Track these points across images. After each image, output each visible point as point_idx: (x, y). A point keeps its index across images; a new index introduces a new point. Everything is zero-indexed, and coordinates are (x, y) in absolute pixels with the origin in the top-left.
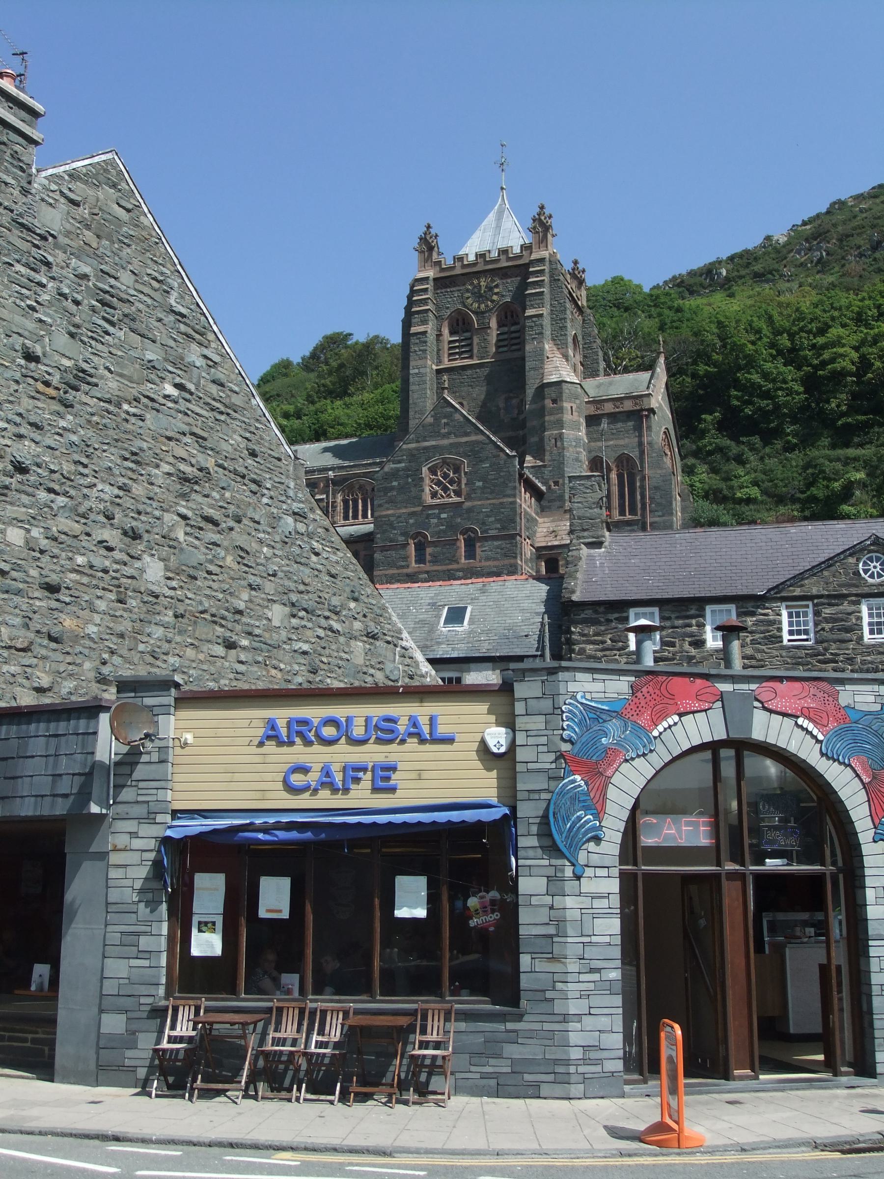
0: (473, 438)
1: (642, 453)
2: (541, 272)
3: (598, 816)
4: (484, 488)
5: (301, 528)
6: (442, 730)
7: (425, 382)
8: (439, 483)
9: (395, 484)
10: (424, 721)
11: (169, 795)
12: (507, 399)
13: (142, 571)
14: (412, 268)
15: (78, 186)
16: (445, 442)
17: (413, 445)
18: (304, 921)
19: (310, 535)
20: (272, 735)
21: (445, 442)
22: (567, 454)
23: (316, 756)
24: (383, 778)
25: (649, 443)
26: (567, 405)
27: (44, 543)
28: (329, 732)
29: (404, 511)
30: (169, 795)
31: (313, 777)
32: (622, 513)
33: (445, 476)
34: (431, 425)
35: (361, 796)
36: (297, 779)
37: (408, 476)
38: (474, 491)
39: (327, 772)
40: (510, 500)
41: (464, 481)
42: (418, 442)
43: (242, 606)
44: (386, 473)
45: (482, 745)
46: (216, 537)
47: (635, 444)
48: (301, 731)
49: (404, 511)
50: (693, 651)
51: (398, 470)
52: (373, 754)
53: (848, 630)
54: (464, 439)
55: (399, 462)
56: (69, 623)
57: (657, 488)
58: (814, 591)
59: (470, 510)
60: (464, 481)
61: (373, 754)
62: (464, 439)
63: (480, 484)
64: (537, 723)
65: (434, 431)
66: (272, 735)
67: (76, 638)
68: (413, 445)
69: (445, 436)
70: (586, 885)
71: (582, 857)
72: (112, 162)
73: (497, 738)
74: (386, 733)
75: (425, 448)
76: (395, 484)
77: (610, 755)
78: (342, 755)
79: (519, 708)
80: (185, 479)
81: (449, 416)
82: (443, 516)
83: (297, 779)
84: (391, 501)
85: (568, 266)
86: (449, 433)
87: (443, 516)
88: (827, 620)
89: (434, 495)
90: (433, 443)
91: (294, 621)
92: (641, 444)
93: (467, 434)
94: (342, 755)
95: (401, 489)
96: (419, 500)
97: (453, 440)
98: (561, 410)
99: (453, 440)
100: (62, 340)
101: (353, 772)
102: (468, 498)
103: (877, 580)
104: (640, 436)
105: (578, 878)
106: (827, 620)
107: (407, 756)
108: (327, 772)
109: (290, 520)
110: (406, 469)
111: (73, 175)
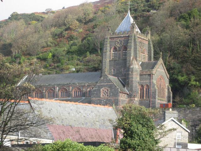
0: (111, 84)
1: (150, 85)
2: (113, 57)
4: (113, 95)
7: (106, 65)
8: (104, 93)
9: (95, 93)
12: (124, 69)
16: (105, 84)
17: (99, 84)
21: (105, 84)
22: (134, 85)
25: (152, 82)
26: (134, 73)
29: (97, 99)
32: (146, 98)
33: (105, 91)
34: (103, 80)
37: (98, 91)
38: (110, 95)
40: (117, 98)
41: (109, 93)
42: (100, 83)
44: (94, 90)
45: (175, 96)
47: (149, 82)
49: (97, 99)
51: (96, 89)
54: (109, 84)
55: (96, 88)
57: (153, 93)
60: (109, 93)
62: (109, 84)
63: (112, 94)
68: (99, 84)
69: (105, 83)
75: (101, 85)
76: (95, 93)
81: (106, 78)
82: (105, 101)
86: (106, 82)
87: (105, 101)
89: (103, 96)
90: (103, 84)
92: (150, 82)
93: (109, 83)
95: (97, 94)
96: (100, 97)
97: (107, 84)
98: (133, 74)
104: (150, 80)
110: (97, 90)
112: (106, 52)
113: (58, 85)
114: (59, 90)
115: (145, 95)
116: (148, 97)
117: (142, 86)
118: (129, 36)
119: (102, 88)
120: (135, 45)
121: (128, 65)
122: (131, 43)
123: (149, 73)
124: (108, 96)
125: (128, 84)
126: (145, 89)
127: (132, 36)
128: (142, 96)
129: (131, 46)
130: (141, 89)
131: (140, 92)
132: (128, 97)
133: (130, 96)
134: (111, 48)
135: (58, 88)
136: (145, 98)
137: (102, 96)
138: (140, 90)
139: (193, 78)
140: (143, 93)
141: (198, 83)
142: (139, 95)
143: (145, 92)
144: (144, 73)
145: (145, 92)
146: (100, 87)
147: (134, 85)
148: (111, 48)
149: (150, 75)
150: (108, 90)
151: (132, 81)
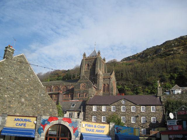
3: (43, 131)
5: (44, 95)
6: (31, 121)
10: (29, 120)
11: (5, 125)
13: (22, 100)
14: (82, 58)
15: (18, 58)
18: (22, 137)
19: (45, 96)
20: (15, 120)
23: (19, 122)
24: (25, 125)
27: (9, 97)
28: (21, 120)
30: (5, 125)
31: (18, 124)
32: (107, 91)
35: (23, 127)
36: (17, 124)
39: (20, 124)
43: (35, 104)
46: (32, 96)
48: (18, 120)
50: (100, 111)
52: (24, 122)
53: (120, 110)
56: (11, 106)
58: (116, 104)
59: (86, 90)
61: (24, 122)
64: (39, 121)
65: (82, 79)
66: (15, 120)
67: (12, 107)
69: (84, 80)
70: (41, 137)
71: (41, 135)
72: (23, 55)
73: (35, 122)
74: (25, 120)
77: (46, 125)
78: (22, 122)
79: (37, 119)
80: (28, 90)
83: (17, 124)
84: (76, 88)
85: (103, 58)
88: (117, 108)
91: (42, 106)
92: (110, 83)
94: (22, 122)
95: (78, 87)
97: (85, 81)
99: (85, 81)
100: (14, 75)
101: (22, 124)
102: (86, 89)
103: (124, 104)
105: (40, 136)
106: (117, 108)
107: (27, 123)
108: (20, 124)
109: (43, 94)
111: (18, 57)
112: (83, 66)
113: (53, 85)
114: (54, 88)
115: (106, 90)
116: (108, 91)
117: (105, 85)
118: (97, 58)
119: (81, 83)
120: (100, 63)
121: (96, 73)
122: (98, 61)
123: (108, 77)
124: (85, 88)
125: (96, 83)
126: (106, 87)
127: (98, 58)
128: (104, 90)
129: (98, 62)
130: (104, 87)
131: (103, 88)
132: (96, 90)
133: (97, 89)
134: (85, 65)
135: (53, 86)
136: (106, 91)
137: (81, 88)
138: (103, 87)
139: (126, 87)
140: (105, 89)
141: (129, 89)
142: (102, 89)
143: (106, 88)
144: (106, 77)
145: (106, 88)
146: (80, 83)
147: (100, 83)
148: (85, 65)
149: (109, 78)
150: (85, 85)
151: (99, 81)
